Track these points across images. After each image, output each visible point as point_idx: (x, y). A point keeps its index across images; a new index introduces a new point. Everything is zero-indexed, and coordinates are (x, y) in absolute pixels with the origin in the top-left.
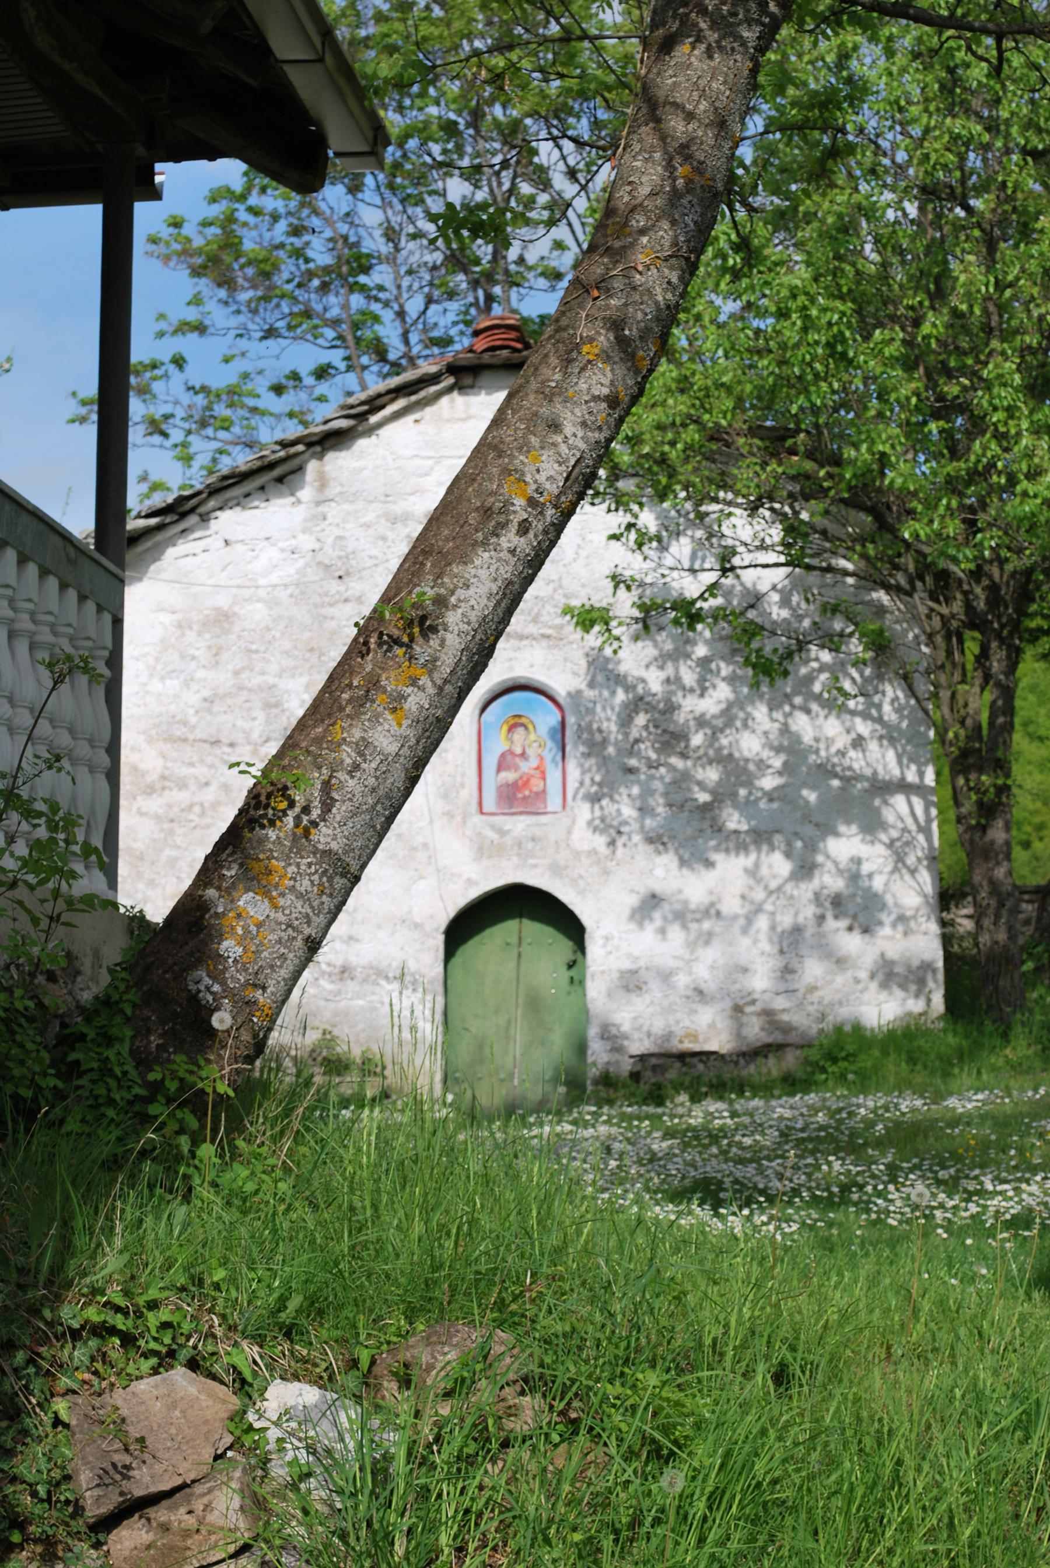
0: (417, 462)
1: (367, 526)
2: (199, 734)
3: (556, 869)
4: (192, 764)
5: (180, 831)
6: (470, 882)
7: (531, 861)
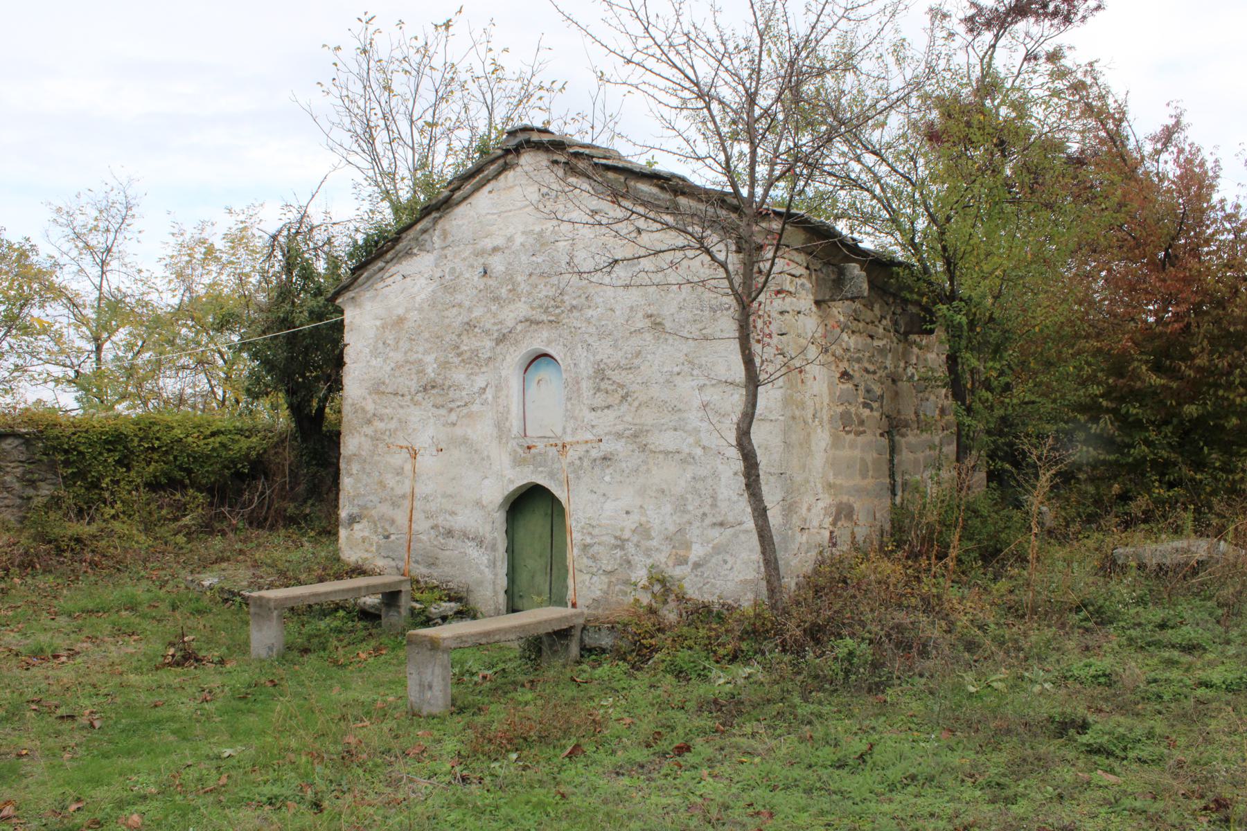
0: (489, 217)
1: (464, 259)
2: (389, 390)
3: (552, 475)
4: (386, 407)
5: (381, 445)
6: (511, 481)
7: (540, 469)
